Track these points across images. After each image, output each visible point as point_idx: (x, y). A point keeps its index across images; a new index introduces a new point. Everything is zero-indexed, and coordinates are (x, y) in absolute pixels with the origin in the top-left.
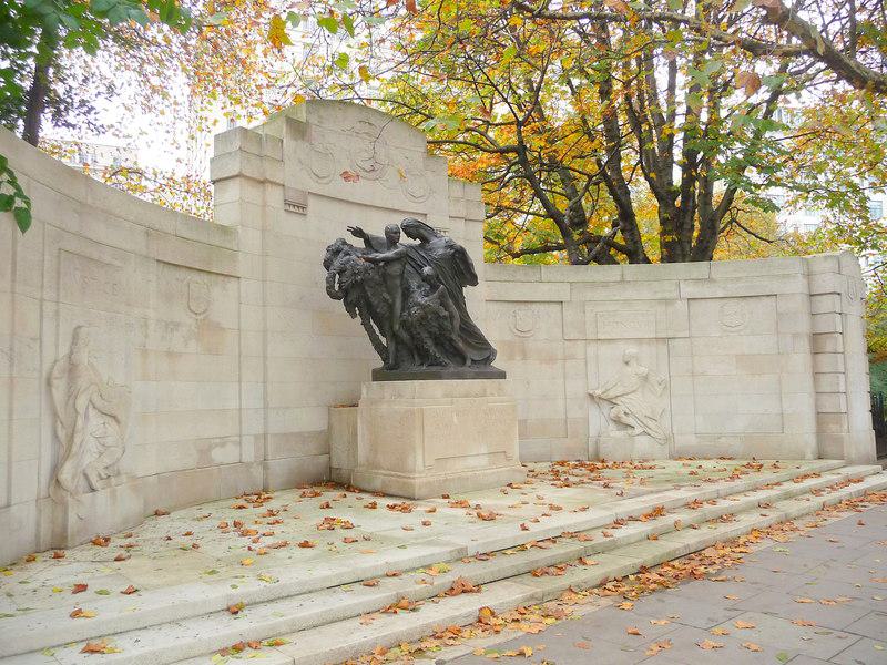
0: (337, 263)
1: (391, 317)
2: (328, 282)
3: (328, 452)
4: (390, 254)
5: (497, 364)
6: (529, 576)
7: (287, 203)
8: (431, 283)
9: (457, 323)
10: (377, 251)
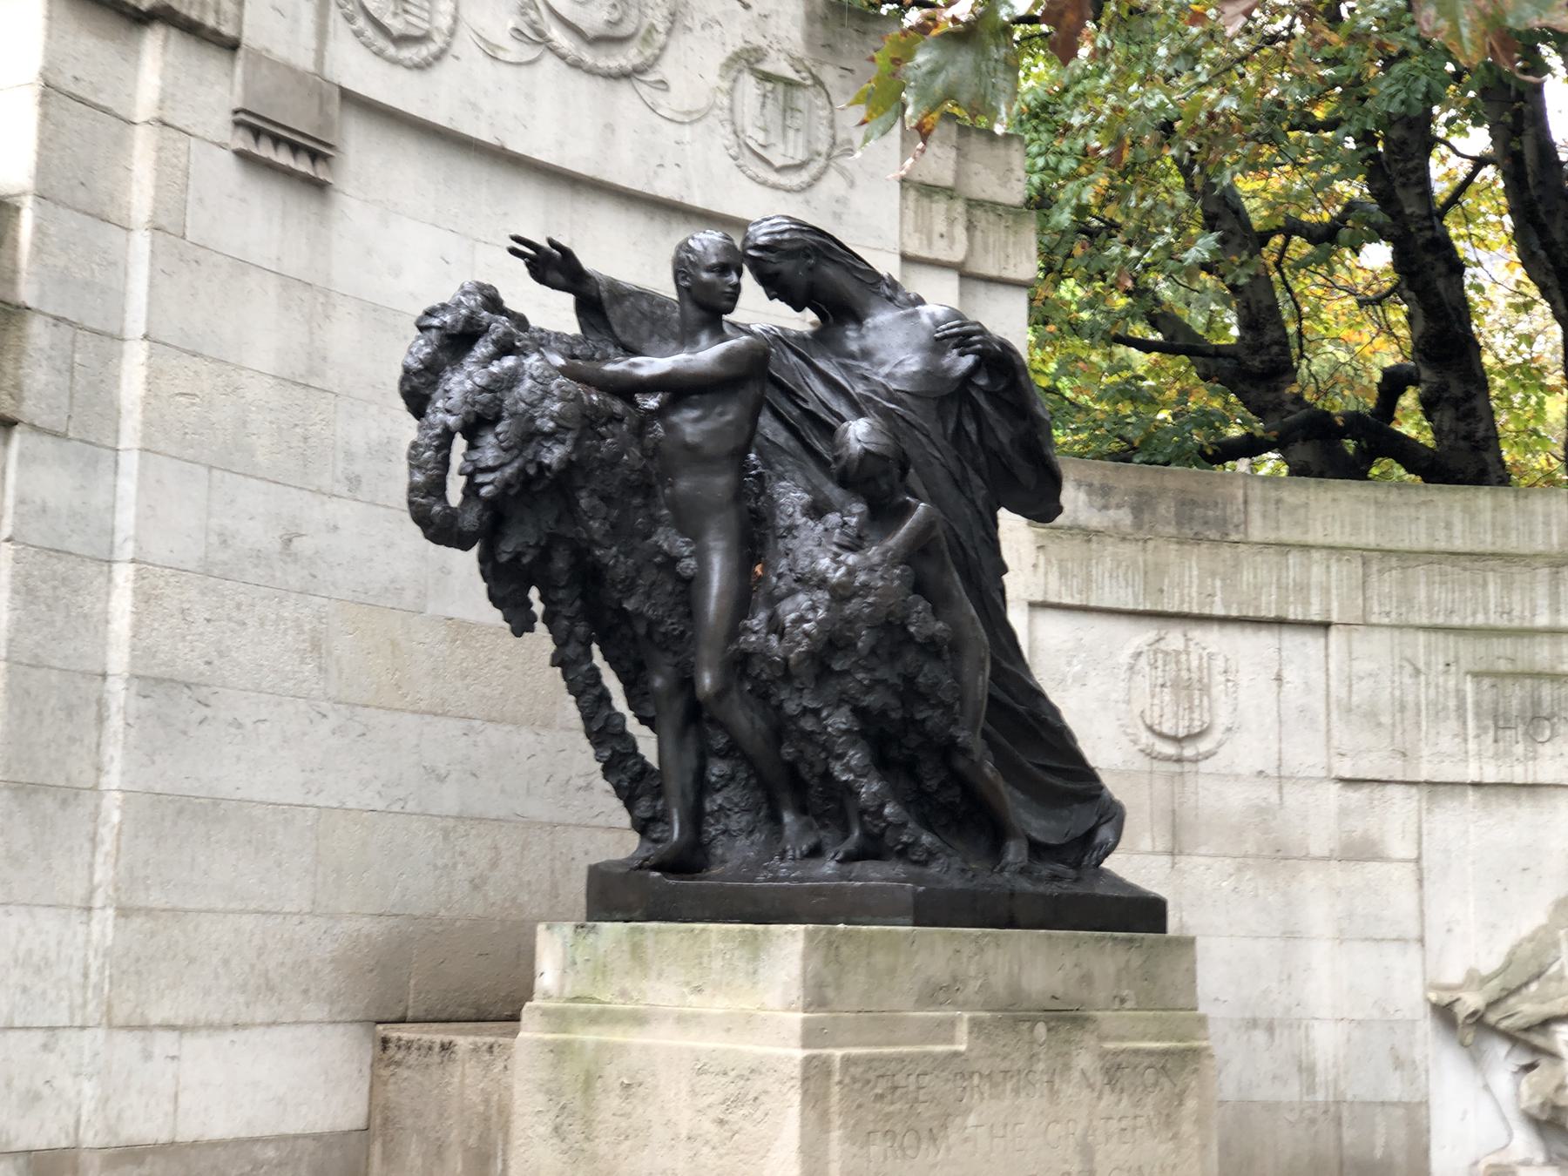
0: (462, 383)
1: (681, 644)
2: (415, 463)
4: (706, 355)
7: (252, 124)
8: (876, 486)
9: (980, 683)
10: (630, 351)
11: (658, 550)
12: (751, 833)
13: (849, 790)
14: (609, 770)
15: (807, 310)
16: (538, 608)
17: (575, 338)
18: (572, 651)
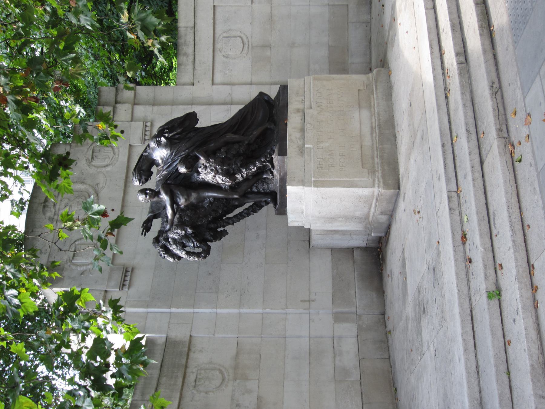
1: (228, 200)
3: (351, 250)
5: (272, 92)
11: (208, 206)
12: (268, 184)
13: (258, 168)
14: (255, 212)
15: (152, 170)
16: (222, 229)
17: (162, 220)
18: (231, 222)
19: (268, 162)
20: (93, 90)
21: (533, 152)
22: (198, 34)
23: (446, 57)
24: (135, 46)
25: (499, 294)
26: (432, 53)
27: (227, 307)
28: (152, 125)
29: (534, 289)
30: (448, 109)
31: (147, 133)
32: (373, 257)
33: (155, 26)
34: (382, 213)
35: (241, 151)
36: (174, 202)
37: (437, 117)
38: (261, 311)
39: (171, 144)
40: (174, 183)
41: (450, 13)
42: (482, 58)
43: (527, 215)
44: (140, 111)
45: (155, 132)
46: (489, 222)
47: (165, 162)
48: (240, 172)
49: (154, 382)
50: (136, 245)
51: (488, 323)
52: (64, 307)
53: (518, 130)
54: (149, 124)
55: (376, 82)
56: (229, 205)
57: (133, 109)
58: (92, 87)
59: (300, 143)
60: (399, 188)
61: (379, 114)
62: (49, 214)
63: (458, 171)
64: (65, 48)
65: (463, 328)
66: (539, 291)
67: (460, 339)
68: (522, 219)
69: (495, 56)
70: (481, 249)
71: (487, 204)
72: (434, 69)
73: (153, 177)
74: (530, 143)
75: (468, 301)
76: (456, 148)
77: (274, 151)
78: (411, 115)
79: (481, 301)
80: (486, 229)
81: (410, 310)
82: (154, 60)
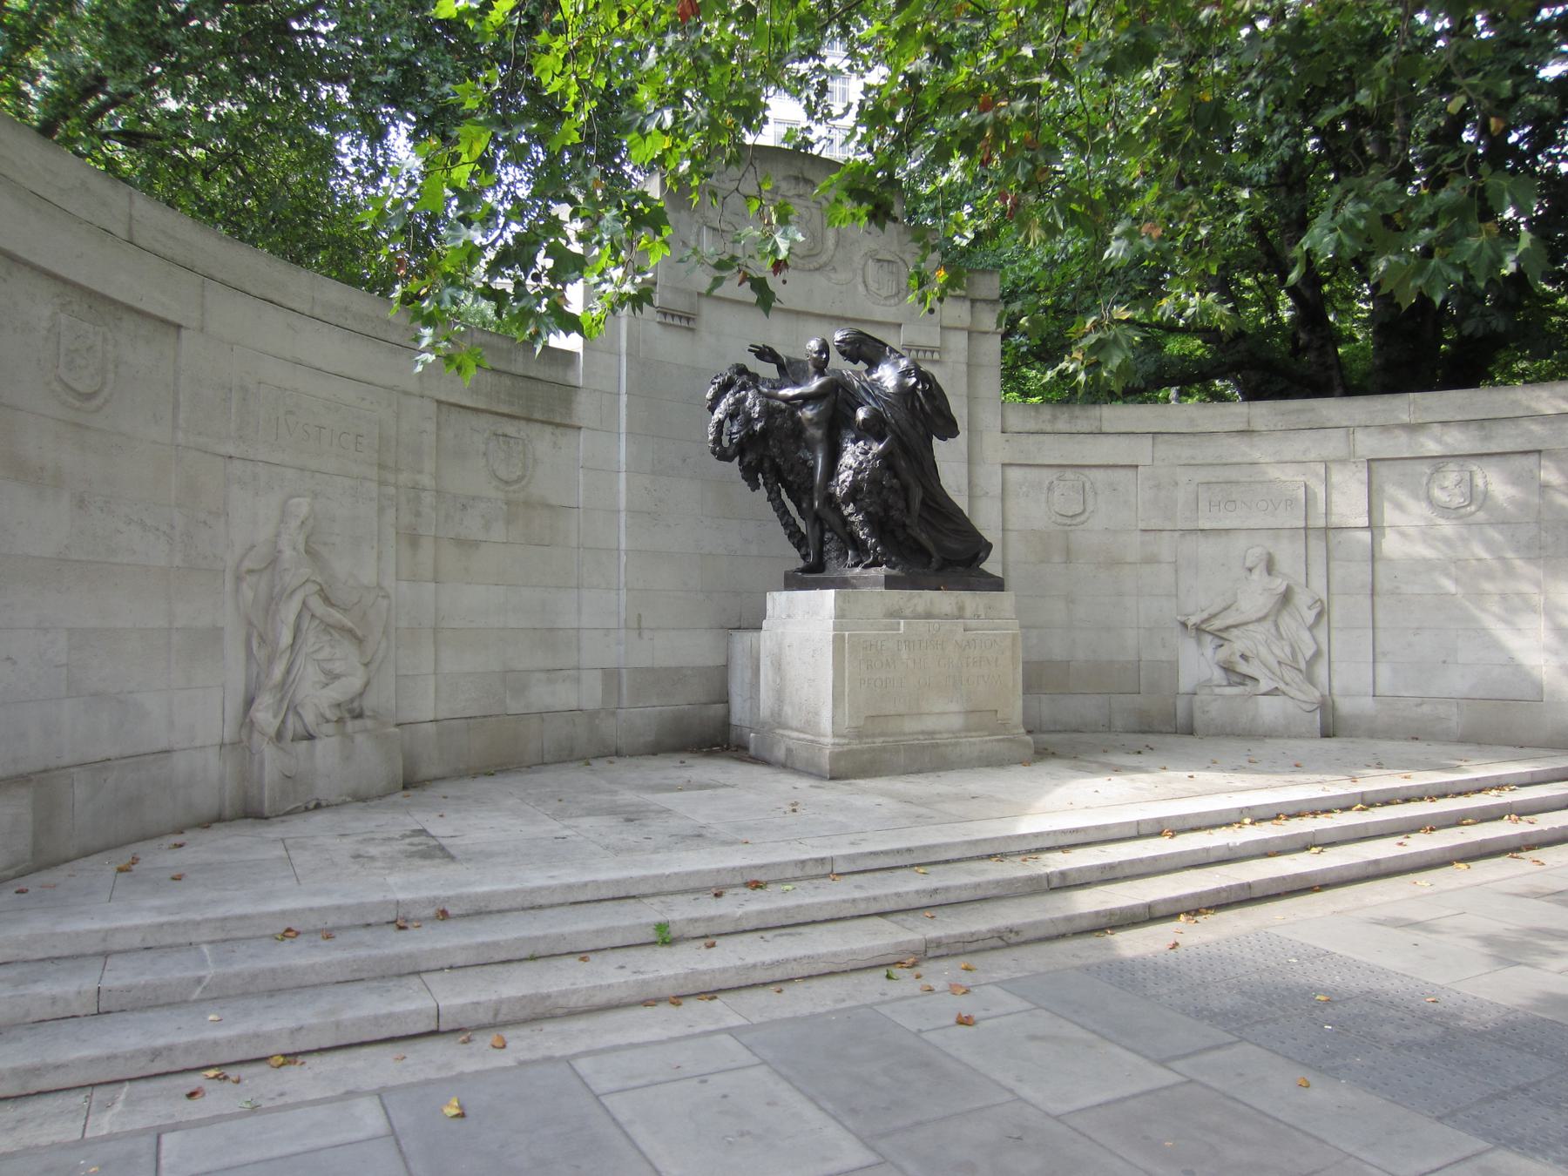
3: (725, 699)
5: (991, 566)
6: (391, 929)
16: (761, 481)
19: (875, 559)
20: (990, 261)
21: (904, 998)
22: (1089, 438)
23: (1058, 855)
24: (1073, 329)
25: (664, 943)
26: (1063, 832)
27: (628, 489)
28: (934, 362)
29: (677, 1000)
30: (971, 859)
31: (921, 354)
32: (715, 735)
33: (1106, 363)
34: (789, 751)
35: (893, 513)
36: (806, 399)
37: (958, 840)
38: (623, 546)
39: (904, 393)
40: (838, 403)
41: (1132, 862)
42: (1057, 915)
43: (799, 989)
44: (959, 341)
45: (924, 367)
46: (784, 927)
47: (875, 384)
48: (858, 512)
49: (502, 366)
50: (732, 335)
51: (616, 924)
52: (641, 210)
53: (941, 973)
54: (936, 356)
55: (1010, 740)
56: (801, 492)
57: (962, 329)
58: (995, 260)
59: (907, 612)
60: (832, 778)
61: (956, 744)
62: (784, 186)
63: (869, 875)
64: (1072, 211)
65: (605, 882)
66: (673, 1009)
67: (588, 877)
68: (792, 980)
69: (1063, 936)
70: (740, 912)
71: (814, 922)
72: (1037, 835)
73: (849, 364)
74: (918, 992)
75: (651, 891)
76: (906, 871)
77: (893, 568)
78: (958, 798)
79: (652, 913)
80: (772, 921)
81: (627, 797)
82: (1038, 365)
